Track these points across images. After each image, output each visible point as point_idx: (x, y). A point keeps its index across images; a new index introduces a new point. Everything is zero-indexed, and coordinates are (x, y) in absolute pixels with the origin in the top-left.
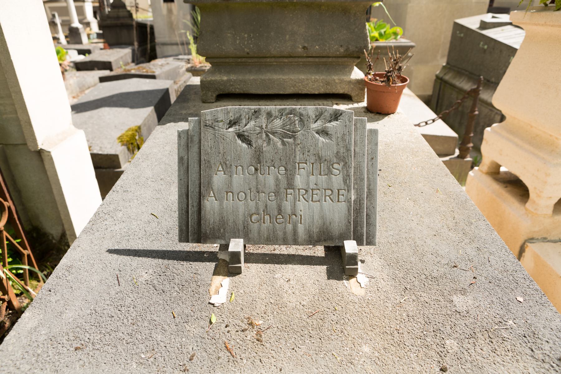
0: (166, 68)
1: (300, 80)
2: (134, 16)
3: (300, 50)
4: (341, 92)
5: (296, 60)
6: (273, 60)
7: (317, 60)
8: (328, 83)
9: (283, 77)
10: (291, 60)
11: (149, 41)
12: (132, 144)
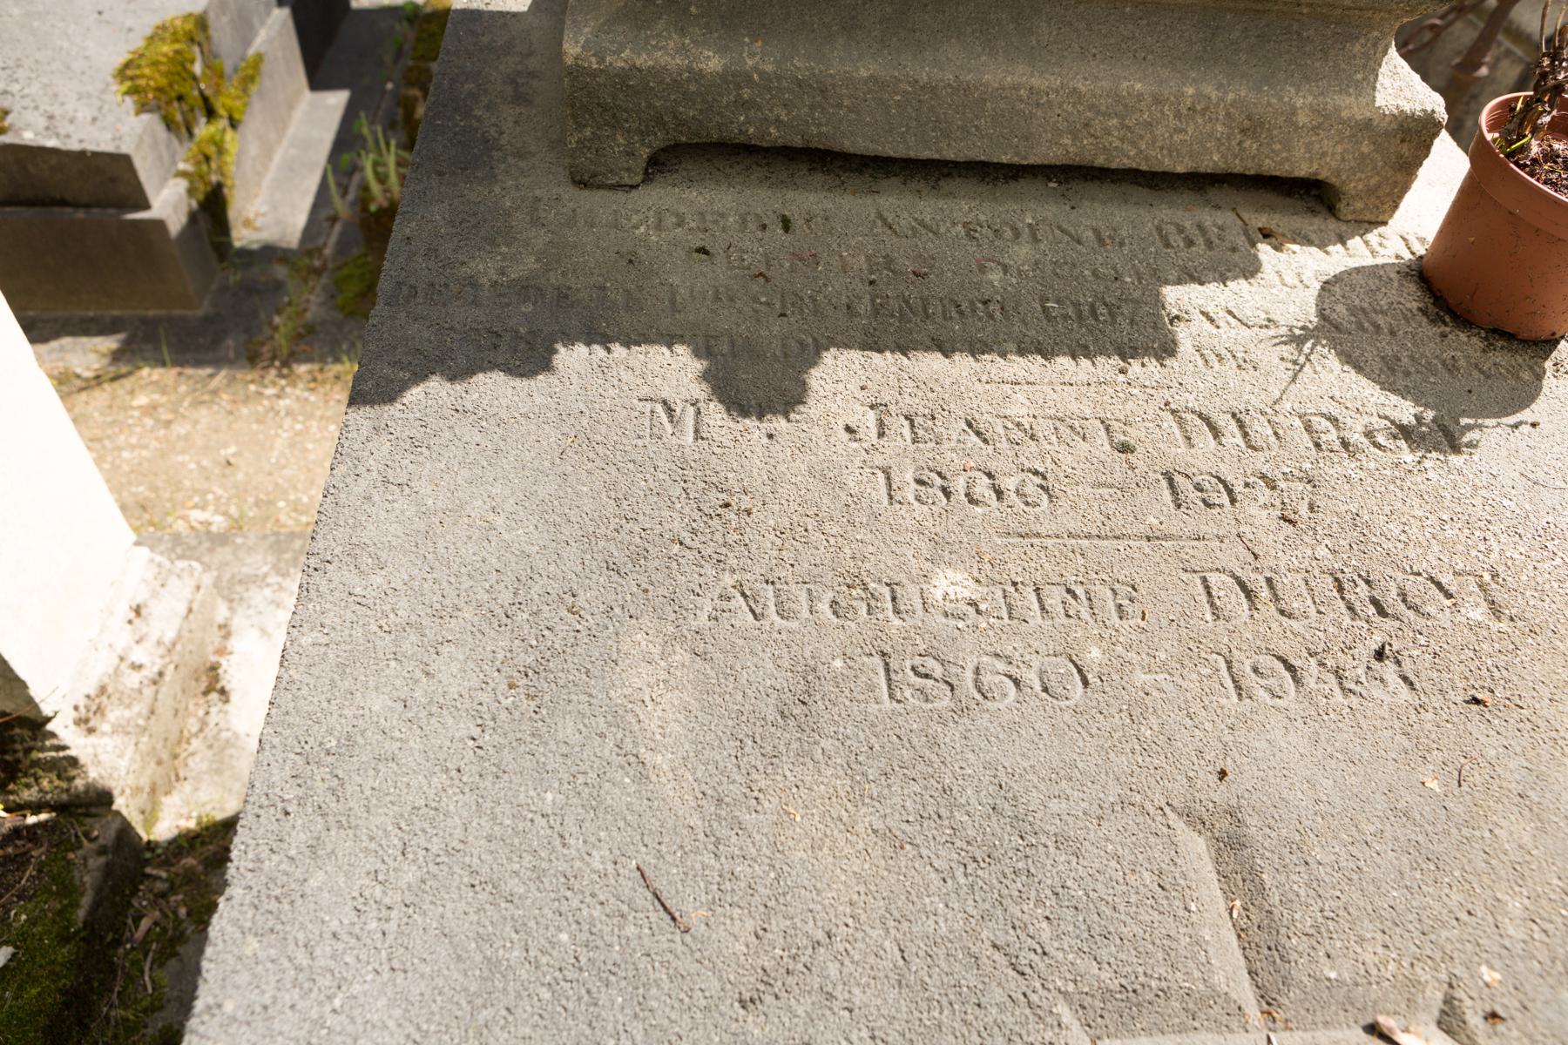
1: (1118, 98)
4: (1303, 170)
8: (1253, 127)
9: (1035, 81)
12: (180, 98)
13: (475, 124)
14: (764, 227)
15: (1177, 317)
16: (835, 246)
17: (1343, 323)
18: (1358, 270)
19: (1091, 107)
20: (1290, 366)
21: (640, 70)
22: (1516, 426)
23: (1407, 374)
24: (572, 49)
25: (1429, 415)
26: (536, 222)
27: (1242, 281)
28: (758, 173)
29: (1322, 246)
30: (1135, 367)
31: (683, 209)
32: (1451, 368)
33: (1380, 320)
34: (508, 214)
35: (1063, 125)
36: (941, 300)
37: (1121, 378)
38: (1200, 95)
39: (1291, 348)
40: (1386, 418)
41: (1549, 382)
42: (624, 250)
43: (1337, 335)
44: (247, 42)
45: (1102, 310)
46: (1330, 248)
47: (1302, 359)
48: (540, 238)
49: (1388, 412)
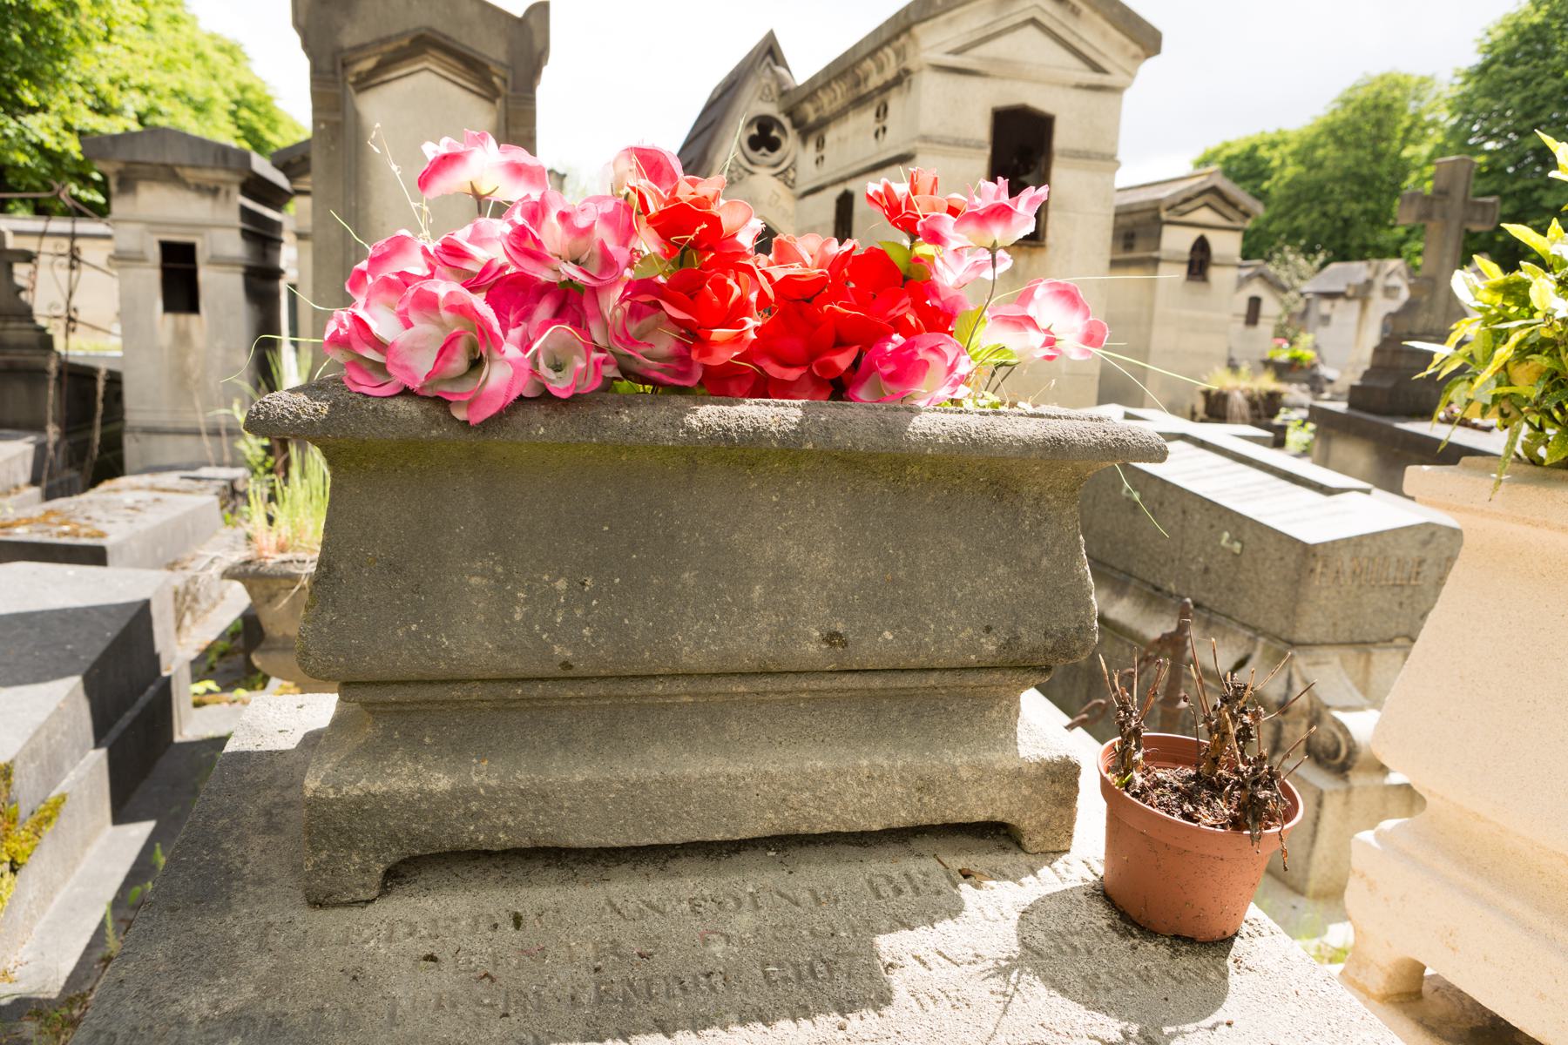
0: (151, 519)
1: (806, 776)
2: (59, 344)
3: (812, 648)
4: (981, 816)
5: (787, 684)
6: (682, 685)
7: (877, 682)
8: (926, 786)
9: (731, 770)
10: (761, 684)
11: (98, 421)
13: (221, 856)
14: (496, 926)
15: (891, 965)
16: (563, 938)
17: (1041, 952)
18: (1050, 897)
19: (784, 785)
20: (1000, 998)
21: (374, 796)
22: (1214, 1028)
23: (1108, 990)
24: (311, 784)
25: (1134, 1029)
26: (262, 947)
27: (948, 921)
28: (495, 875)
29: (1016, 879)
30: (854, 1021)
31: (416, 918)
32: (1146, 978)
33: (1076, 941)
34: (235, 943)
35: (763, 803)
36: (665, 978)
37: (841, 1034)
38: (873, 765)
39: (999, 980)
40: (1096, 1038)
41: (1233, 979)
42: (350, 967)
43: (1039, 961)
44: (52, 784)
45: (820, 967)
46: (1023, 880)
47: (1010, 990)
48: (263, 965)
49: (1096, 1031)
